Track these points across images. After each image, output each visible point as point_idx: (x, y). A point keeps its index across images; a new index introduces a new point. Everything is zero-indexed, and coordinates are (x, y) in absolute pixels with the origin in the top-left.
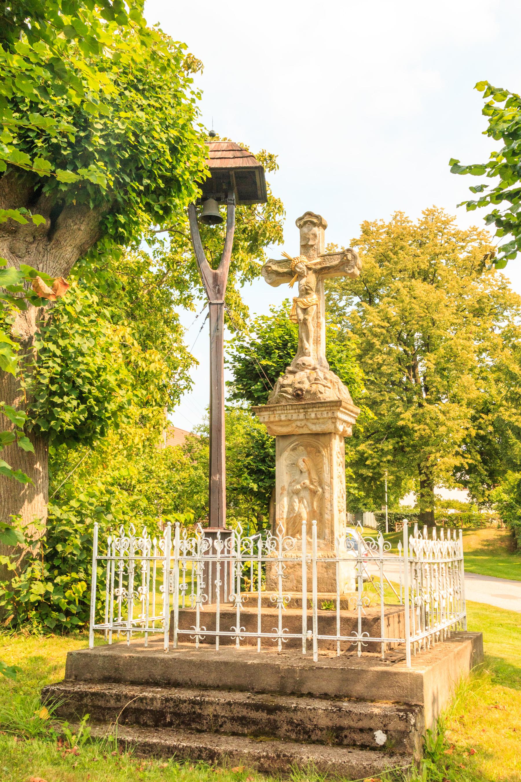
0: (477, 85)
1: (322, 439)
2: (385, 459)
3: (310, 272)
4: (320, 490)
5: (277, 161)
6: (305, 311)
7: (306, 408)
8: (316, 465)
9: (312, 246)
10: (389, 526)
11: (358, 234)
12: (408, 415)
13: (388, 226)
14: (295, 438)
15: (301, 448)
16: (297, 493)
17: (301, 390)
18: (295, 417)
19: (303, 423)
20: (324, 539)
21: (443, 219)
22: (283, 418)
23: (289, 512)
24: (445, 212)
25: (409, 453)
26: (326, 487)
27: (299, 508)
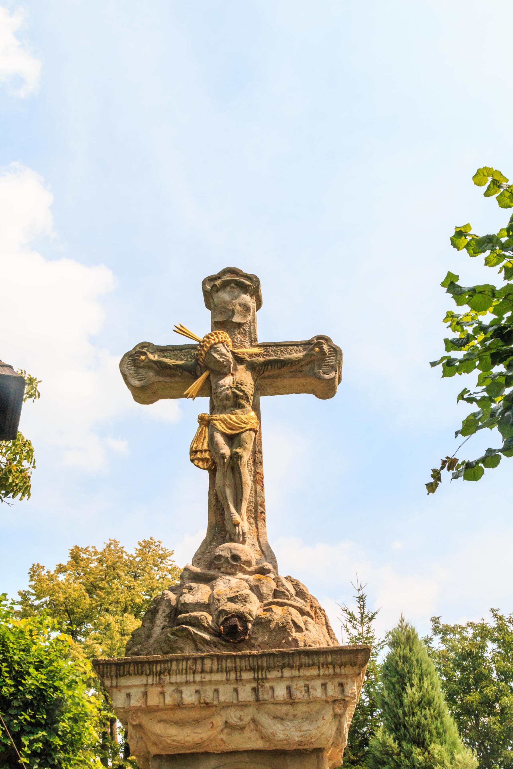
0: (479, 172)
3: (240, 367)
5: (40, 388)
6: (233, 439)
7: (260, 666)
9: (240, 325)
11: (66, 560)
13: (101, 553)
17: (241, 617)
18: (226, 694)
19: (247, 715)
21: (161, 552)
22: (189, 696)
24: (162, 545)
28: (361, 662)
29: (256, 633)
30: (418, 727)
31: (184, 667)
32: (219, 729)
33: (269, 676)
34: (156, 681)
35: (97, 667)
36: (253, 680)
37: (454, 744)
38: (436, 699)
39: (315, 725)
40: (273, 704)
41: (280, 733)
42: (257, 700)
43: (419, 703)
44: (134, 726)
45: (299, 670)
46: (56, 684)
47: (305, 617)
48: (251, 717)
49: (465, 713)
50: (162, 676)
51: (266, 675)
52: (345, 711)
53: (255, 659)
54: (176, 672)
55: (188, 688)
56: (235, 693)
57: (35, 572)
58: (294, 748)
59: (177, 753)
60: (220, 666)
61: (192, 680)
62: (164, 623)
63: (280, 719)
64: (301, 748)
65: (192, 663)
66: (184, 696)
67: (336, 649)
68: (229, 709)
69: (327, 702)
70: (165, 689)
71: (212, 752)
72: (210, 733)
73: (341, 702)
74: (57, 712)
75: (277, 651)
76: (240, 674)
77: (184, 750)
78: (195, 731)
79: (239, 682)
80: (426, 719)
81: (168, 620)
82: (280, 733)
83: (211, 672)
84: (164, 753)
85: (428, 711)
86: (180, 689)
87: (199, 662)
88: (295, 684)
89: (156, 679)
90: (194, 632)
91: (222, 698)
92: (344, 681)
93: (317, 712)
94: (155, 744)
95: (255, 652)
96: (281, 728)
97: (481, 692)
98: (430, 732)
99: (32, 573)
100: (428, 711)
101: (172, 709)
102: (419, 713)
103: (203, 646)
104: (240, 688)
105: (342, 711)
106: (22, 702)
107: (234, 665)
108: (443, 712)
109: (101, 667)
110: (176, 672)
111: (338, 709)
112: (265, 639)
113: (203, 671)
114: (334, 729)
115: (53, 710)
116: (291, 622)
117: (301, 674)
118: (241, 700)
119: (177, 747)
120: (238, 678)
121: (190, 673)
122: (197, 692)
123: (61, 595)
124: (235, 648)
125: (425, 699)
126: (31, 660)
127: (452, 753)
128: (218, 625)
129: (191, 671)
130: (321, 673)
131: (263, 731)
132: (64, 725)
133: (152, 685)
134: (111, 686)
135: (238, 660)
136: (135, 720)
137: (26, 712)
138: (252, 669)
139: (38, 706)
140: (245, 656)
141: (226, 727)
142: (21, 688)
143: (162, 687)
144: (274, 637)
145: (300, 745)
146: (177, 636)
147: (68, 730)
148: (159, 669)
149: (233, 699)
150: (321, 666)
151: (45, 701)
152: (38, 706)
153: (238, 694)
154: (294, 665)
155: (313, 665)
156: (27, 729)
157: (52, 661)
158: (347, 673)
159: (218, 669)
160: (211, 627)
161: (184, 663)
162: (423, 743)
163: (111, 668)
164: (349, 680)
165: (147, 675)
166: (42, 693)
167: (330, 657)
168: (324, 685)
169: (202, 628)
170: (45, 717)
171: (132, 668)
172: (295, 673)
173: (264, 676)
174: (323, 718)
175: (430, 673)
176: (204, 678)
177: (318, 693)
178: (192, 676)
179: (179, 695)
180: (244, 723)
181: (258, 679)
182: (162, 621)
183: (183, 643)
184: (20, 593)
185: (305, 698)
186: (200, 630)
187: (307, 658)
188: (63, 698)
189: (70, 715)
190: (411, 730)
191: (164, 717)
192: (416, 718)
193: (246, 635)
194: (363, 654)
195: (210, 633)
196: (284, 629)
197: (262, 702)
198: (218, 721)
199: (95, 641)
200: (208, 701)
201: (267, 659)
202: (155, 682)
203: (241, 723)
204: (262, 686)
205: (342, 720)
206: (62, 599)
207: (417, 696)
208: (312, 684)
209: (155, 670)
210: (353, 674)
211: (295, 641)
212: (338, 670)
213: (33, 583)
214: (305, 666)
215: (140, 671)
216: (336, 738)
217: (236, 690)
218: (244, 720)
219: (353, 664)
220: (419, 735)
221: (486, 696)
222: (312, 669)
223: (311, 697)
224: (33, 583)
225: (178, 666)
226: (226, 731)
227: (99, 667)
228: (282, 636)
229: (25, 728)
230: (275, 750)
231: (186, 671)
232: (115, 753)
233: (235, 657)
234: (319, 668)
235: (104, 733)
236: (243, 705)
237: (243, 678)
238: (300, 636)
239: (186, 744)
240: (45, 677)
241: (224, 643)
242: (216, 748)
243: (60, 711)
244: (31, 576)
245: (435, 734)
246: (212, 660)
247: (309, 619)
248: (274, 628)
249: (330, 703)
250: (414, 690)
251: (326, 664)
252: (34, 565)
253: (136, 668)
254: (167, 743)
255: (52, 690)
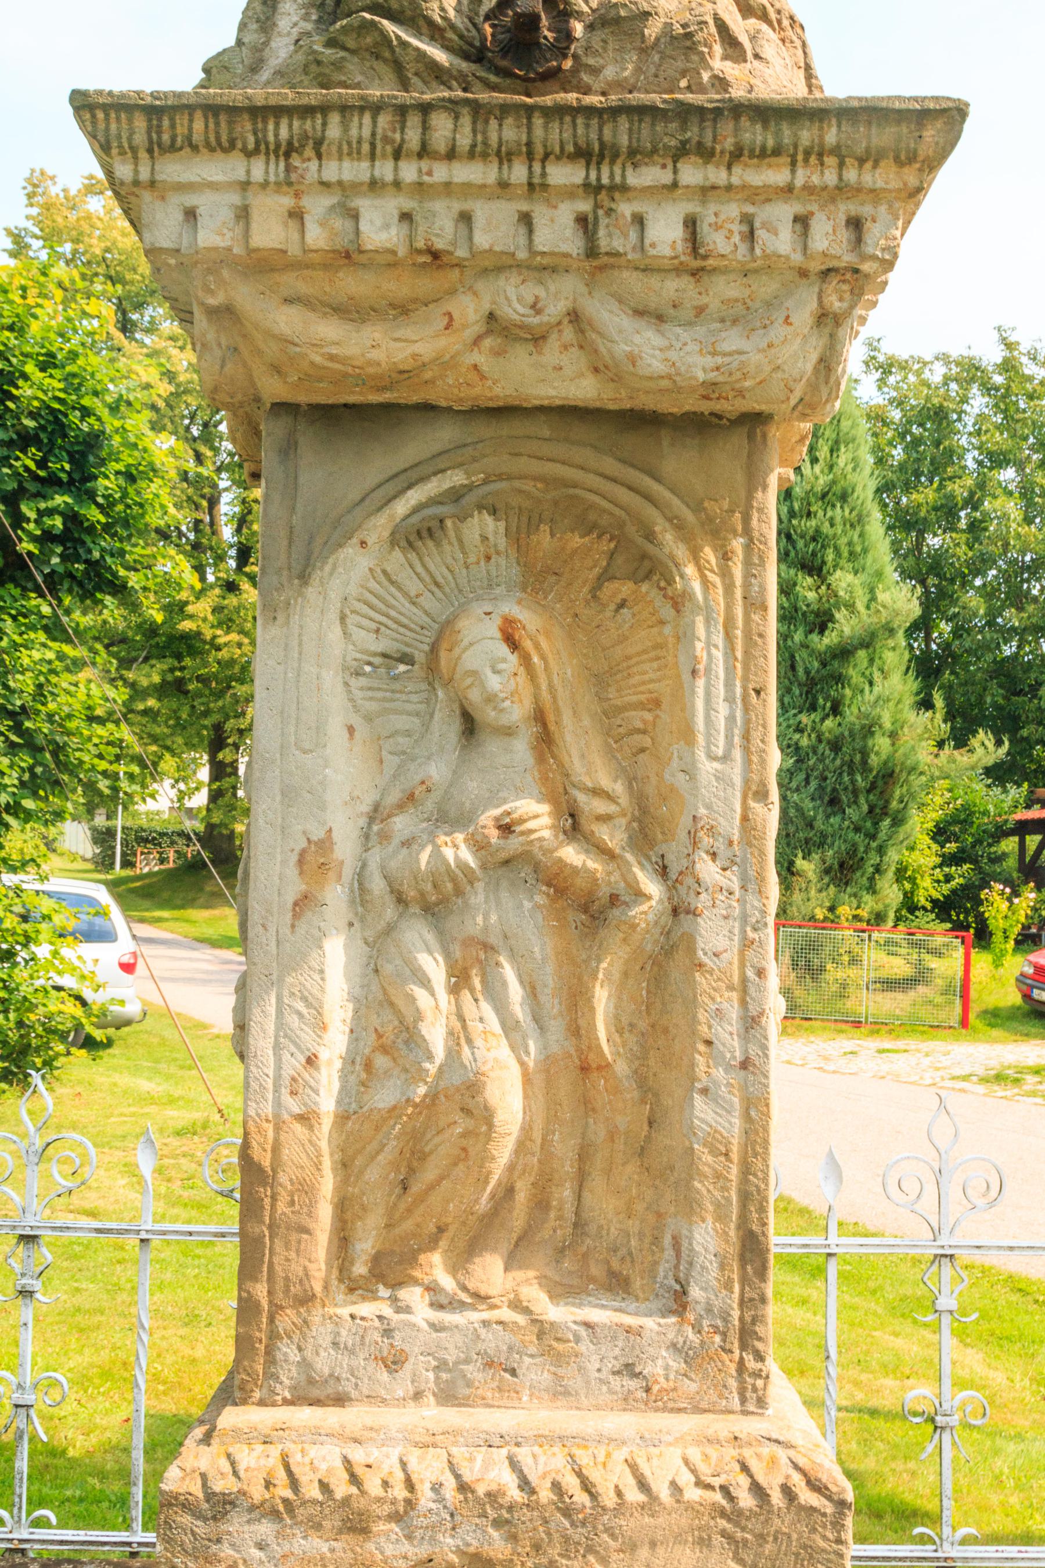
1: (678, 461)
2: (141, 707)
4: (652, 887)
8: (601, 679)
10: (124, 854)
12: (202, 608)
14: (446, 434)
15: (482, 527)
16: (435, 902)
18: (494, 228)
19: (559, 295)
20: (678, 1301)
22: (379, 227)
23: (361, 1069)
25: (199, 694)
26: (708, 870)
27: (460, 1034)
28: (931, 153)
29: (596, 53)
30: (814, 539)
31: (366, 132)
32: (470, 334)
33: (633, 179)
34: (277, 175)
35: (88, 116)
36: (581, 190)
37: (879, 574)
38: (859, 489)
39: (759, 340)
40: (636, 269)
41: (653, 356)
42: (592, 251)
43: (824, 496)
44: (213, 312)
45: (729, 167)
46: (86, 402)
47: (753, 21)
48: (570, 305)
49: (906, 523)
50: (296, 161)
51: (623, 176)
52: (852, 307)
53: (595, 122)
54: (340, 148)
55: (377, 202)
56: (523, 230)
57: (35, 186)
58: (687, 408)
59: (342, 401)
60: (479, 138)
61: (389, 177)
62: (302, 24)
63: (655, 316)
64: (705, 407)
65: (392, 122)
66: (364, 226)
67: (855, 104)
68: (502, 277)
69: (803, 273)
70: (306, 202)
71: (443, 404)
72: (442, 342)
73: (848, 276)
74: (91, 458)
75: (665, 101)
76: (544, 167)
77: (361, 393)
78: (400, 333)
79: (535, 196)
80: (832, 525)
81: (314, 17)
82: (653, 356)
83: (451, 155)
84: (302, 398)
85: (838, 509)
86: (353, 205)
87: (414, 120)
88: (711, 212)
89: (277, 170)
90: (398, 37)
91: (482, 240)
92: (866, 210)
93: (768, 304)
94: (277, 369)
95: (594, 100)
96: (657, 341)
97: (941, 486)
98: (836, 549)
99: (30, 189)
100: (838, 509)
101: (325, 267)
102: (820, 513)
103: (425, 82)
104: (541, 214)
105: (845, 305)
106: (18, 433)
107: (524, 138)
108: (868, 515)
109: (100, 115)
110: (340, 148)
111: (834, 298)
112: (626, 74)
113: (424, 151)
114: (814, 357)
115: (83, 455)
116: (711, 22)
117: (735, 180)
118: (541, 248)
119: (340, 380)
120: (536, 180)
121: (384, 156)
122: (406, 217)
123: (95, 241)
124: (528, 86)
125: (837, 489)
126: (28, 349)
127: (872, 591)
128: (475, 25)
129: (389, 149)
130: (799, 182)
131: (603, 350)
132: (107, 484)
133: (265, 185)
134: (136, 183)
135: (538, 121)
136: (212, 292)
137: (25, 453)
138: (583, 154)
139: (52, 442)
140: (561, 111)
141: (489, 332)
142: (11, 405)
143: (297, 195)
144: (652, 70)
145: (706, 397)
146: (344, 48)
147: (117, 496)
148: (284, 133)
149: (517, 247)
150: (800, 157)
151: (65, 436)
152: (52, 442)
153: (531, 232)
154: (718, 147)
155: (777, 152)
156: (32, 487)
157: (73, 356)
158: (880, 184)
159: (474, 146)
160: (452, 27)
161: (367, 119)
162: (820, 569)
163: (130, 121)
164: (883, 209)
165: (249, 154)
166: (56, 418)
167: (834, 130)
168: (802, 222)
169: (425, 30)
170: (67, 467)
171: (198, 125)
172: (717, 175)
173: (618, 179)
174: (787, 320)
175: (854, 440)
176: (430, 173)
177: (781, 241)
178: (389, 164)
179: (349, 224)
180: (545, 319)
181: (599, 188)
182: (295, 19)
183: (363, 73)
184: (9, 232)
185: (740, 258)
186: (419, 34)
187: (758, 127)
188: (103, 432)
189: (120, 467)
190: (800, 544)
191: (303, 288)
192: (813, 523)
193: (565, 56)
194: (939, 124)
195: (447, 48)
196: (688, 43)
197: (605, 259)
198: (469, 309)
199: (170, 343)
200: (439, 245)
201: (631, 122)
202: (272, 178)
203: (535, 320)
204: (610, 212)
205: (841, 332)
206: (98, 251)
207: (821, 481)
208: (763, 214)
209: (271, 138)
210: (899, 190)
211: (721, 82)
212: (851, 175)
213: (34, 211)
214: (752, 155)
215: (224, 138)
216: (813, 387)
217: (526, 219)
218: (547, 311)
219: (905, 159)
220: (814, 554)
221: (952, 496)
222: (770, 166)
223: (758, 252)
224: (34, 211)
225: (346, 129)
226: (488, 342)
227: (94, 116)
228: (680, 64)
229: (26, 485)
230: (632, 410)
231: (373, 146)
232: (220, 558)
233: (530, 110)
234: (793, 164)
235: (198, 522)
236: (546, 267)
237: (551, 180)
238: (736, 73)
239: (371, 370)
240: (61, 385)
241: (493, 78)
242: (456, 391)
243: (97, 456)
244: (30, 196)
245: (846, 554)
246: (457, 118)
247: (764, 27)
248: (657, 39)
249: (813, 278)
250: (817, 469)
251: (818, 153)
252: (33, 171)
253: (211, 126)
254: (312, 363)
255: (78, 413)
